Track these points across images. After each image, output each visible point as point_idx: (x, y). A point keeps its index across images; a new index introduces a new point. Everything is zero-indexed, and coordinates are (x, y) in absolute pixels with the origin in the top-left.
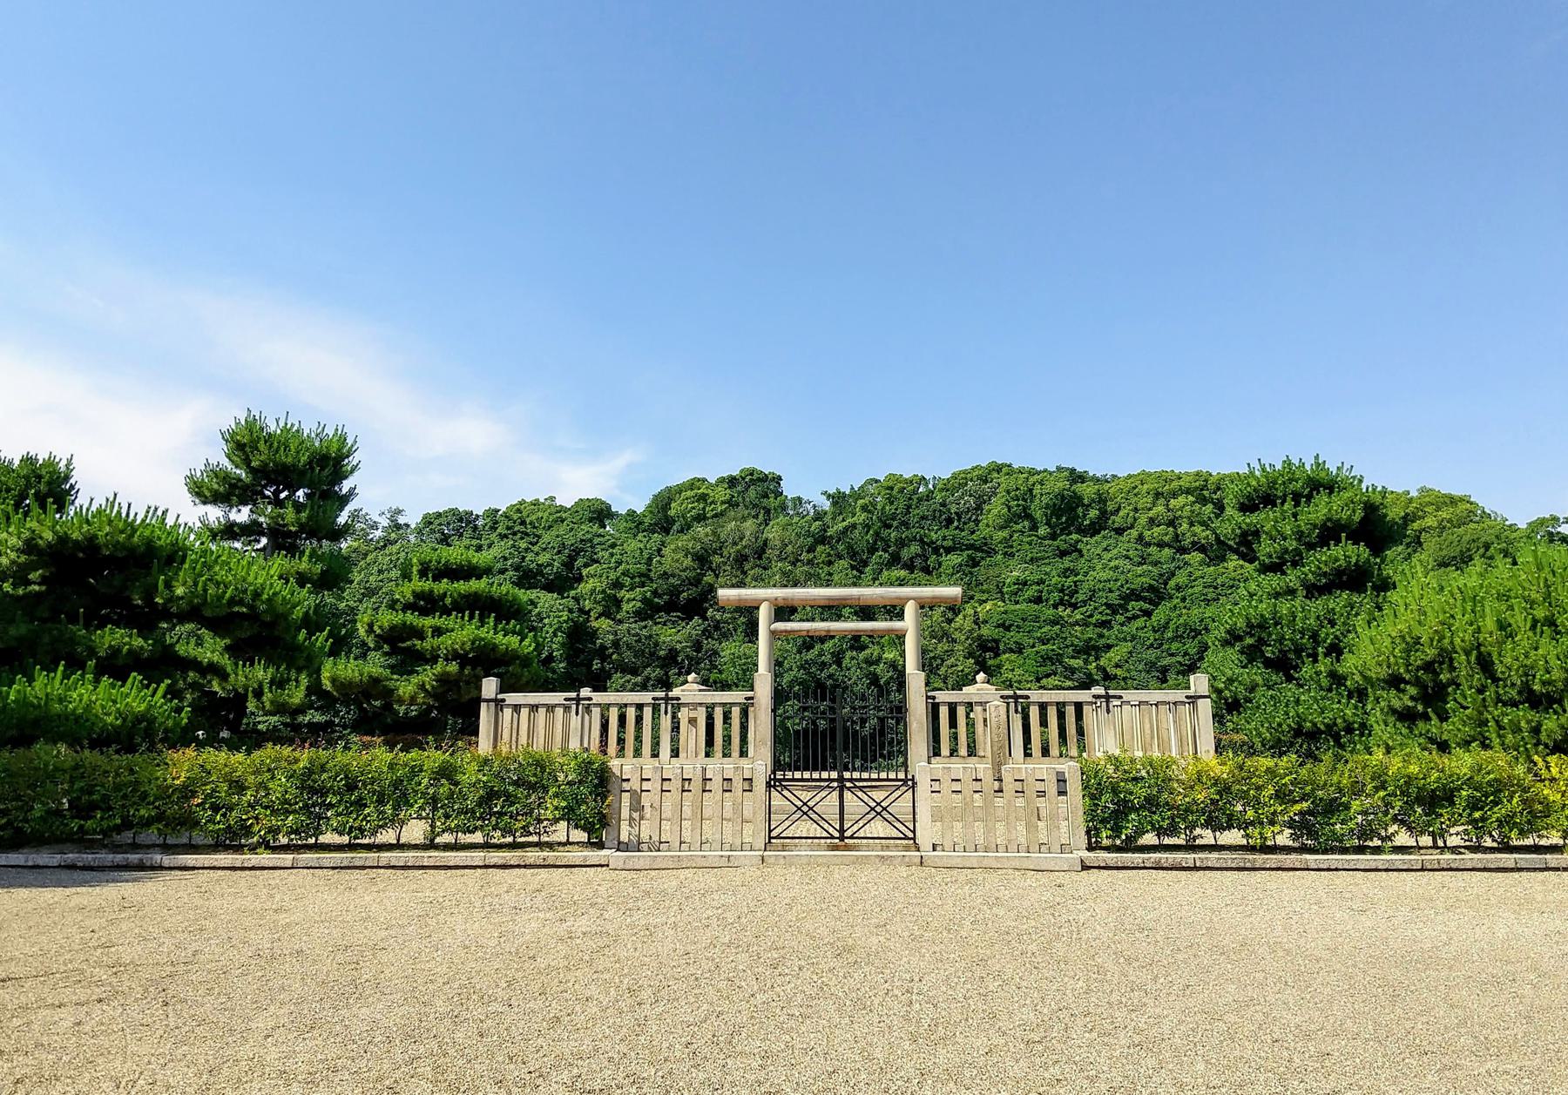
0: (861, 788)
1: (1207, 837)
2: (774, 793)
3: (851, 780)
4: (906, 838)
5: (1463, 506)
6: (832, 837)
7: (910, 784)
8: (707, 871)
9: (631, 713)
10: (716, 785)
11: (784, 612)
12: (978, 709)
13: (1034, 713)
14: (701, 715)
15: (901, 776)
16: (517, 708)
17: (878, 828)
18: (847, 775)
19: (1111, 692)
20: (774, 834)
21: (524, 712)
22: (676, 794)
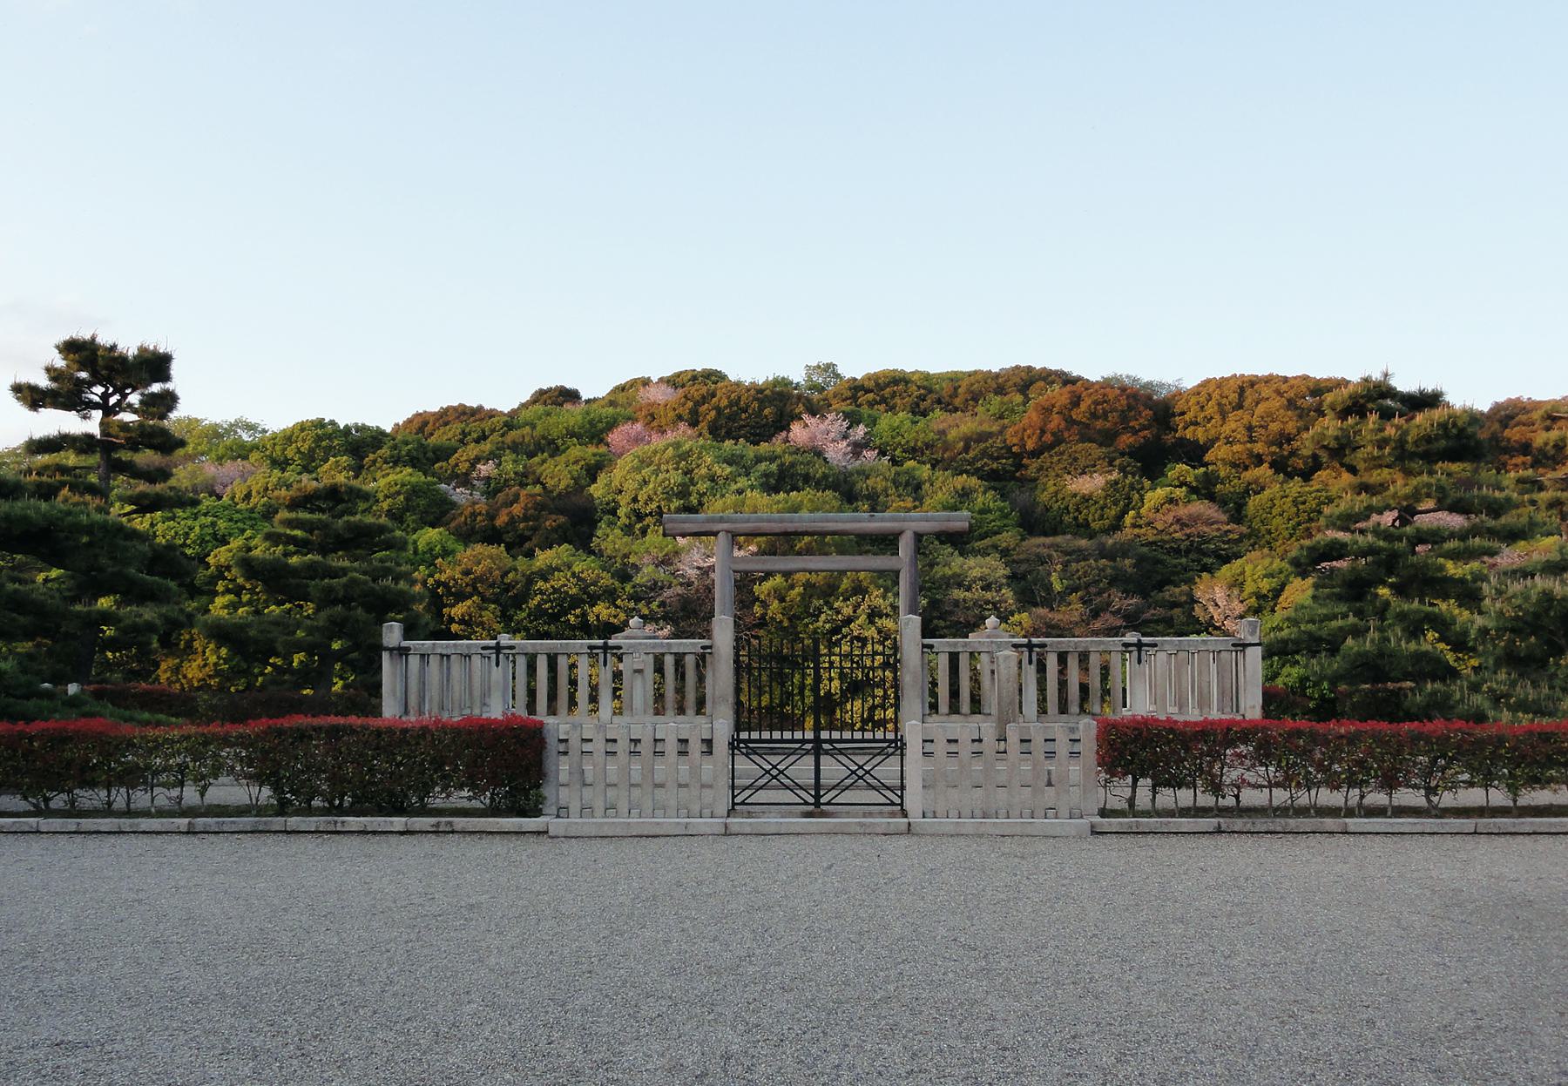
0: (841, 752)
1: (1377, 798)
2: (740, 759)
3: (831, 741)
4: (893, 804)
6: (806, 803)
7: (899, 746)
8: (656, 844)
12: (984, 658)
13: (1052, 663)
14: (648, 664)
15: (890, 736)
16: (424, 657)
18: (824, 735)
21: (434, 661)
22: (622, 756)
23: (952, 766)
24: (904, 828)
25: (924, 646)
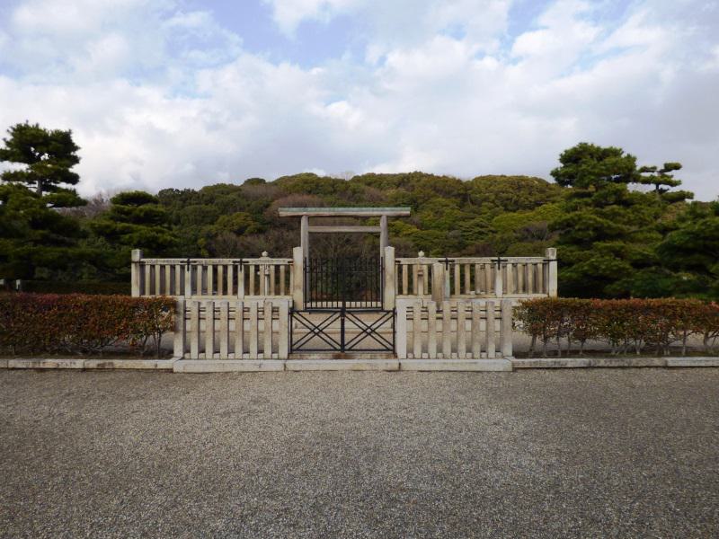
4: (388, 350)
5: (609, 160)
6: (336, 349)
9: (220, 269)
10: (253, 314)
11: (313, 220)
13: (457, 269)
17: (369, 342)
19: (449, 259)
20: (295, 347)
23: (424, 325)
24: (396, 367)
25: (396, 261)
